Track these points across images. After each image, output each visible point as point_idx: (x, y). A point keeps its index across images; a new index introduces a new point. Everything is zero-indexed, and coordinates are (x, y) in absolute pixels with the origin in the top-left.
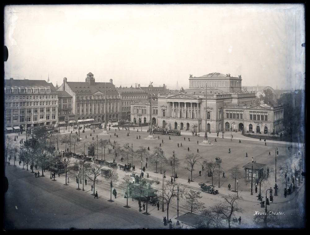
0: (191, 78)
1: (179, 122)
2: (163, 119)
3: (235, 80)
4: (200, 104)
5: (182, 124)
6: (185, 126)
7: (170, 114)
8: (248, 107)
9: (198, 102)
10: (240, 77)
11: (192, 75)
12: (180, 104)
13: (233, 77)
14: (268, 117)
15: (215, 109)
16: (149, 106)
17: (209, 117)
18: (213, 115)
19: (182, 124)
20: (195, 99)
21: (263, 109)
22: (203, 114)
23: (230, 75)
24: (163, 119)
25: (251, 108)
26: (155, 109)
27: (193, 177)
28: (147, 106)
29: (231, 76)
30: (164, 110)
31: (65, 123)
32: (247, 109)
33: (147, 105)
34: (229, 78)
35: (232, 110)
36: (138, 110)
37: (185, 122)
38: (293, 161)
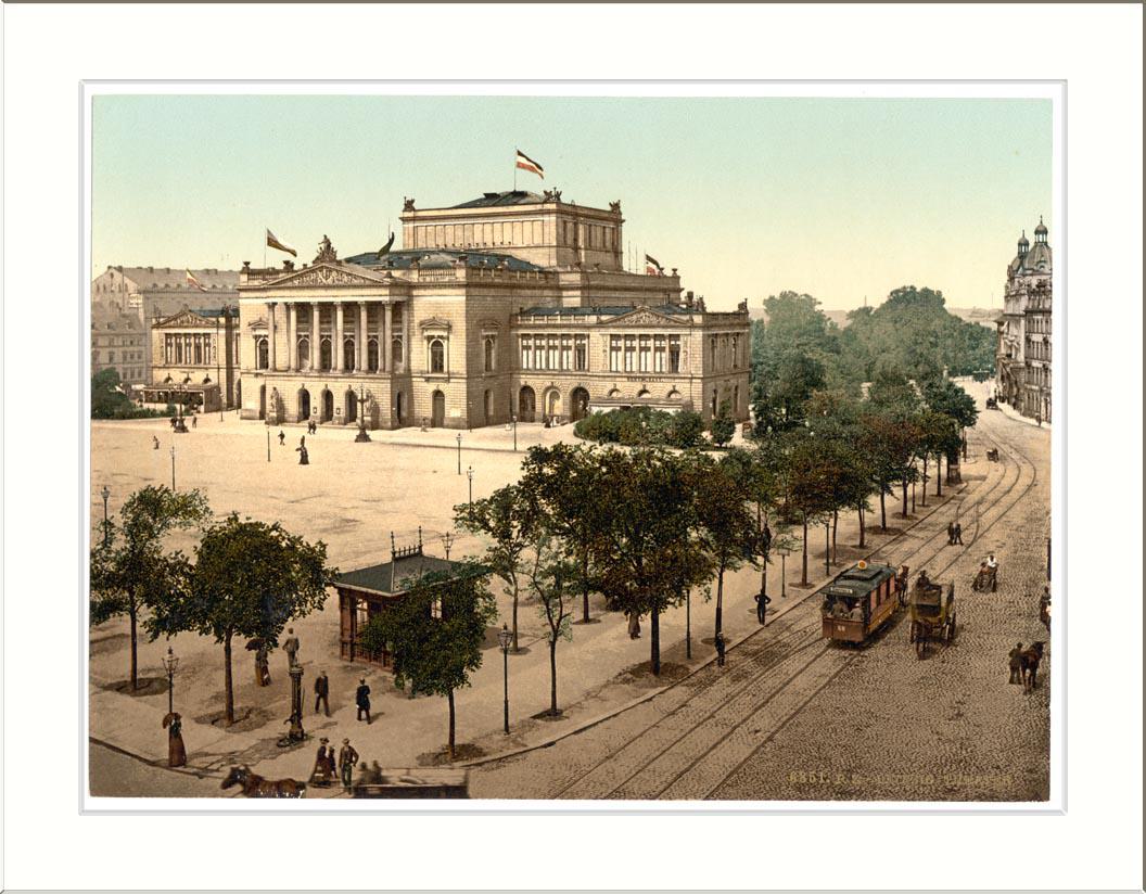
1: (316, 391)
2: (432, 387)
3: (593, 217)
4: (398, 309)
5: (328, 396)
6: (316, 402)
7: (180, 354)
9: (387, 299)
10: (616, 206)
11: (413, 201)
14: (682, 355)
15: (460, 326)
17: (437, 365)
18: (456, 355)
19: (328, 396)
20: (376, 287)
21: (721, 321)
24: (260, 382)
25: (615, 321)
26: (192, 340)
27: (128, 636)
28: (214, 331)
29: (565, 199)
30: (437, 344)
32: (600, 325)
33: (683, 325)
34: (553, 206)
35: (546, 332)
36: (179, 346)
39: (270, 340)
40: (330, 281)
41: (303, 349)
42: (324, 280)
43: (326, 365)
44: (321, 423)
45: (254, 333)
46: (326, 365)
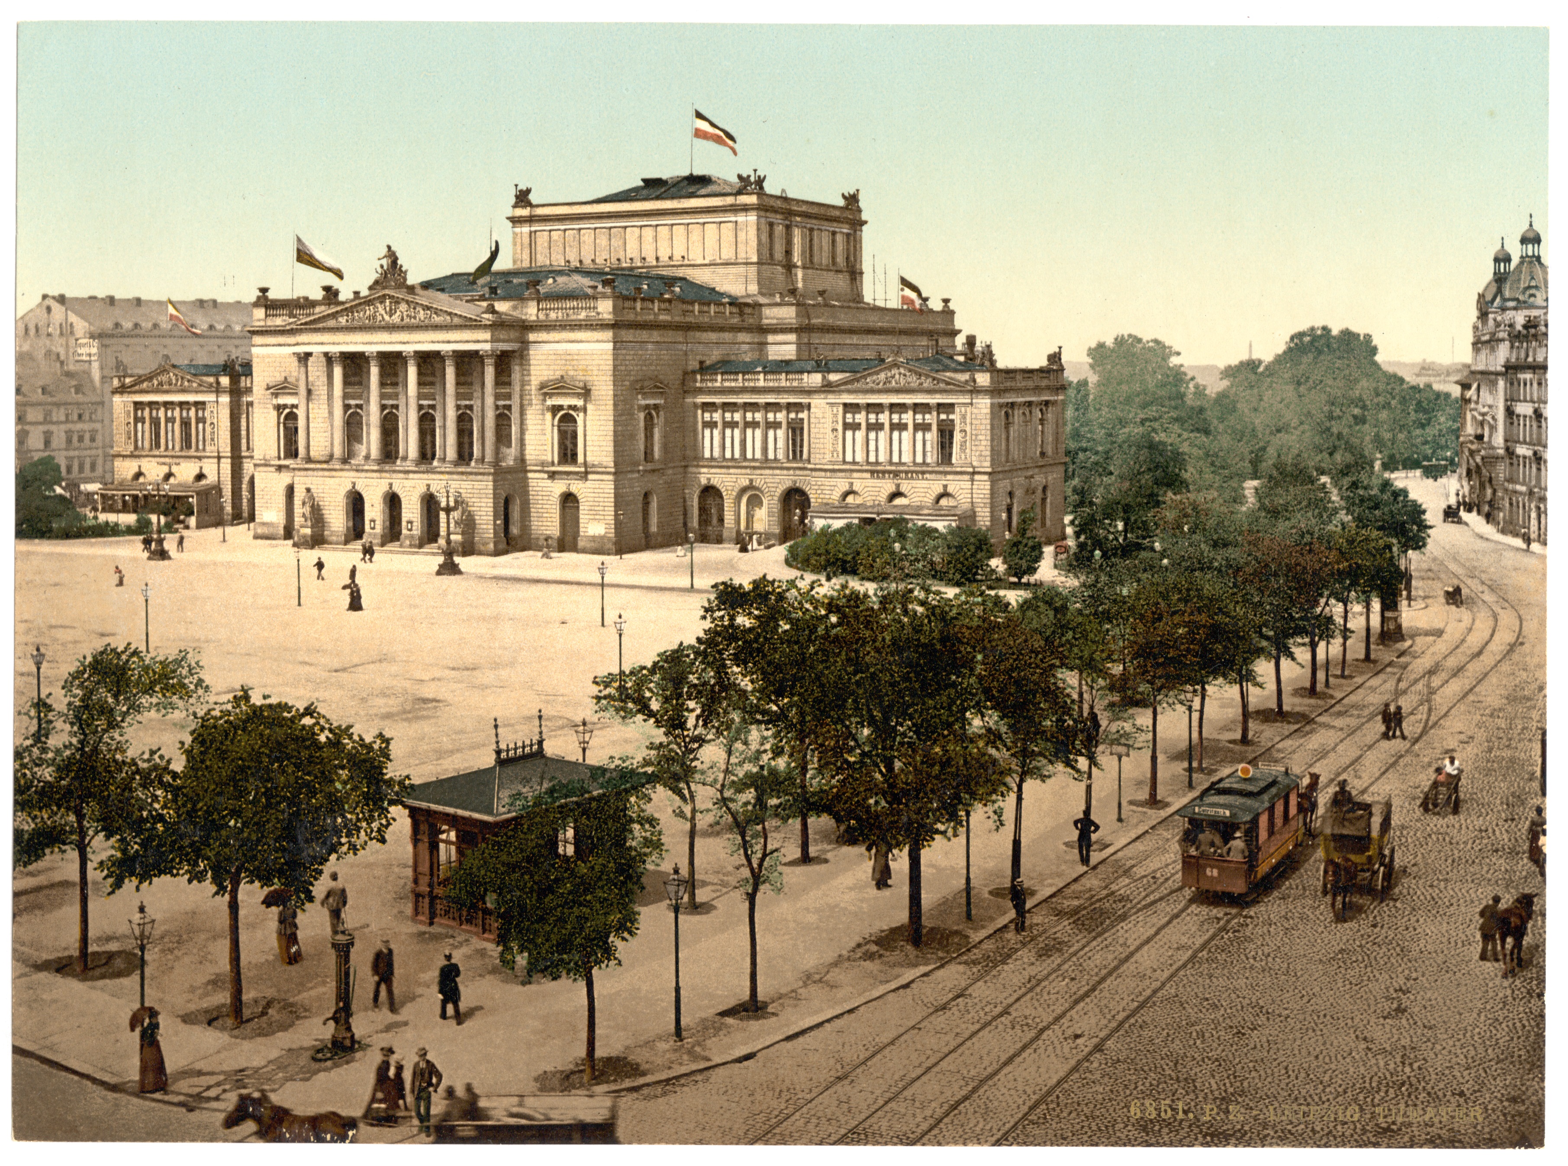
0: (525, 212)
4: (504, 362)
5: (393, 501)
6: (412, 512)
8: (833, 377)
9: (487, 347)
10: (852, 199)
11: (528, 191)
12: (382, 367)
13: (790, 195)
15: (604, 389)
16: (225, 399)
17: (568, 450)
19: (393, 501)
22: (539, 438)
23: (760, 182)
27: (73, 884)
29: (770, 188)
31: (457, 559)
32: (828, 388)
34: (753, 199)
35: (762, 399)
37: (411, 490)
38: (650, 809)
39: (301, 413)
40: (396, 318)
41: (353, 427)
42: (387, 318)
43: (389, 452)
44: (383, 545)
45: (275, 402)
46: (389, 452)
